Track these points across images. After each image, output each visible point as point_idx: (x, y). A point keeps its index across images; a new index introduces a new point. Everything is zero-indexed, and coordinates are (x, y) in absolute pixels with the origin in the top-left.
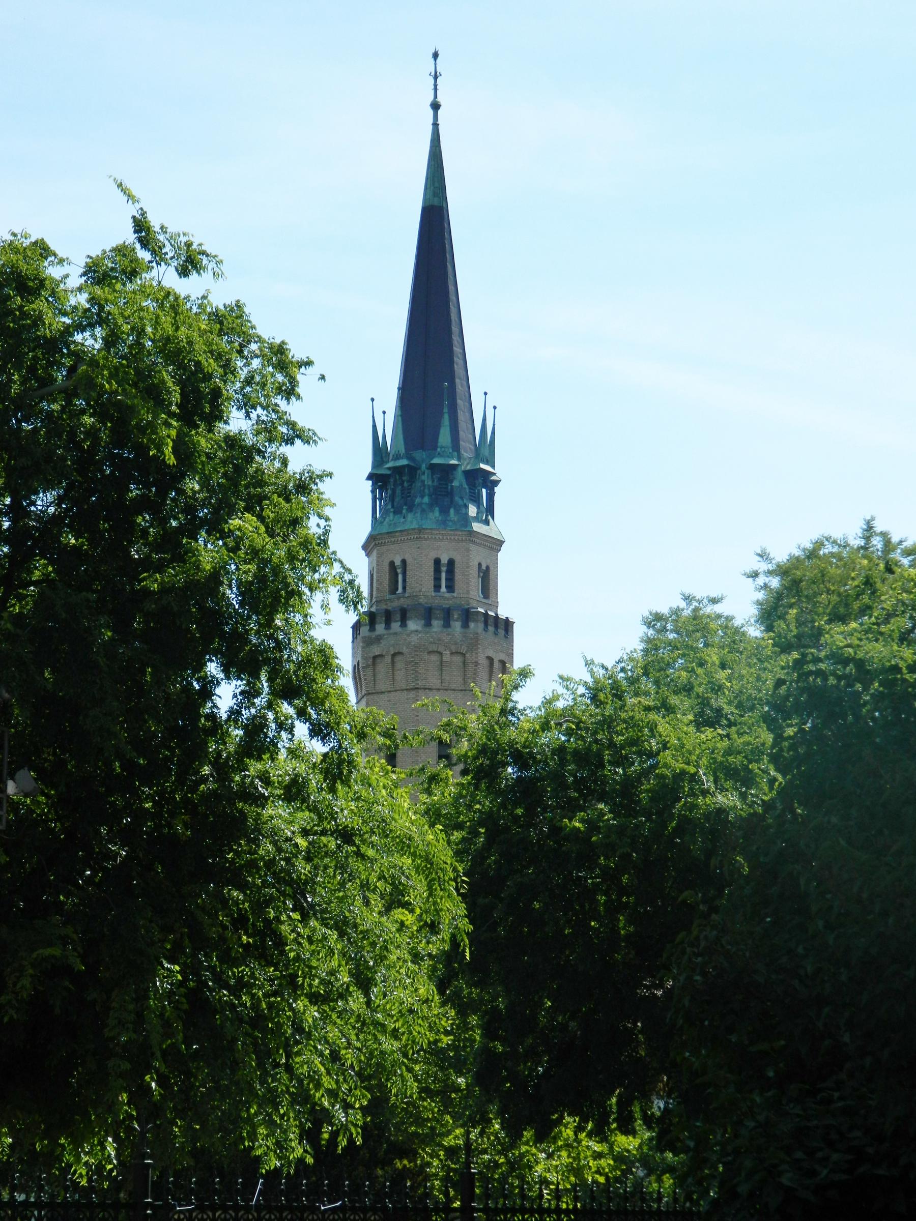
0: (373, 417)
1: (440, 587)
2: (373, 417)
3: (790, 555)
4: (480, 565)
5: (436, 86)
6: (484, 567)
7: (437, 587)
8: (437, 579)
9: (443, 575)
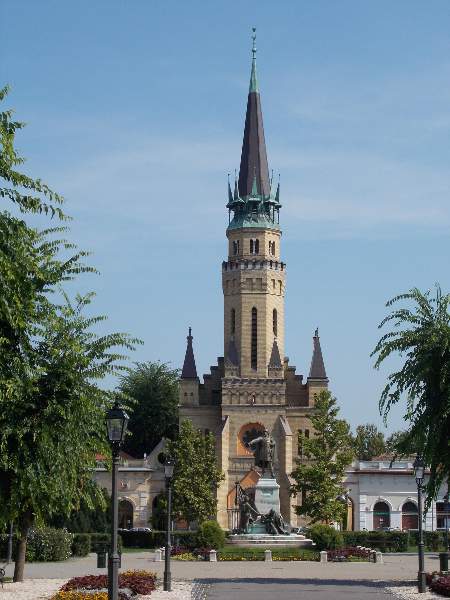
0: (279, 185)
1: (253, 251)
2: (279, 185)
3: (330, 392)
4: (270, 241)
5: (190, 332)
6: (272, 242)
7: (251, 251)
8: (251, 248)
9: (254, 247)
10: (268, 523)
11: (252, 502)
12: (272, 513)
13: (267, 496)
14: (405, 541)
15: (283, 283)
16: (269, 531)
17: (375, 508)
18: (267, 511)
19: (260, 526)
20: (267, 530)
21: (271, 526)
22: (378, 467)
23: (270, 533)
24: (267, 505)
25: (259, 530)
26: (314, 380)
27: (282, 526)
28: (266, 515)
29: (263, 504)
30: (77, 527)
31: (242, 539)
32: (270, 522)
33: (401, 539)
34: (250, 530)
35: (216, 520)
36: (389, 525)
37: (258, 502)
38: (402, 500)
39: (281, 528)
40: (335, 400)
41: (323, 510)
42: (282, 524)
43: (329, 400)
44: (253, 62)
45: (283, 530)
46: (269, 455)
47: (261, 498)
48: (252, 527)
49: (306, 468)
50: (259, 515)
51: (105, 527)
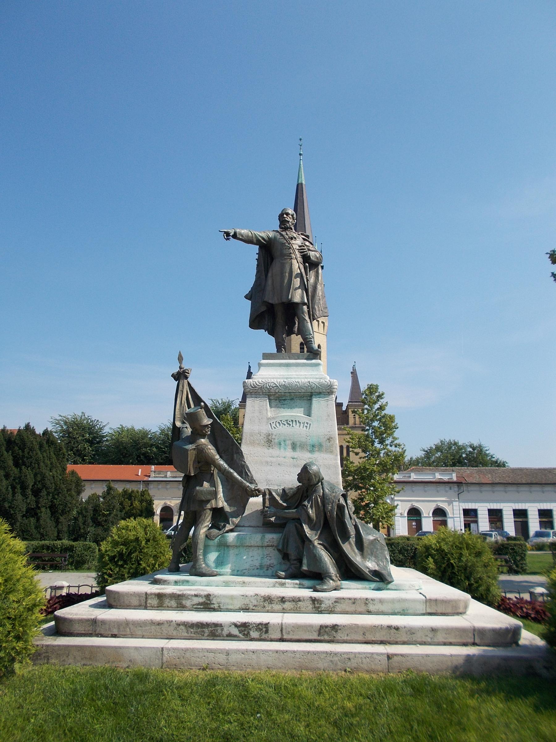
10: (291, 527)
11: (230, 448)
12: (308, 480)
13: (289, 422)
14: (523, 555)
15: (326, 324)
16: (296, 564)
17: (408, 513)
18: (290, 480)
19: (256, 538)
20: (285, 556)
21: (304, 539)
22: (410, 477)
23: (296, 574)
24: (289, 453)
25: (251, 558)
26: (353, 403)
27: (353, 540)
28: (284, 494)
29: (275, 452)
30: (34, 531)
31: (160, 606)
32: (298, 521)
33: (516, 552)
34: (213, 556)
35: (503, 529)
36: (421, 529)
37: (253, 443)
38: (433, 506)
39: (349, 549)
40: (383, 394)
41: (375, 511)
42: (352, 532)
43: (377, 394)
44: (300, 162)
45: (356, 558)
46: (297, 282)
47: (265, 428)
48: (223, 546)
49: (355, 465)
50: (256, 493)
51: (89, 532)
